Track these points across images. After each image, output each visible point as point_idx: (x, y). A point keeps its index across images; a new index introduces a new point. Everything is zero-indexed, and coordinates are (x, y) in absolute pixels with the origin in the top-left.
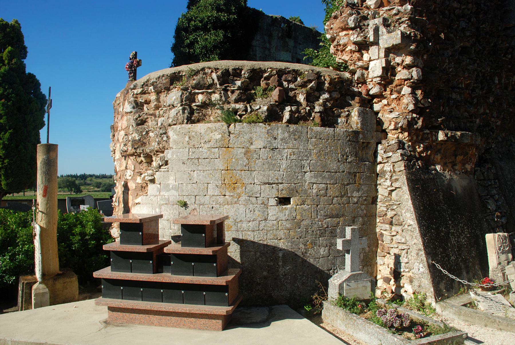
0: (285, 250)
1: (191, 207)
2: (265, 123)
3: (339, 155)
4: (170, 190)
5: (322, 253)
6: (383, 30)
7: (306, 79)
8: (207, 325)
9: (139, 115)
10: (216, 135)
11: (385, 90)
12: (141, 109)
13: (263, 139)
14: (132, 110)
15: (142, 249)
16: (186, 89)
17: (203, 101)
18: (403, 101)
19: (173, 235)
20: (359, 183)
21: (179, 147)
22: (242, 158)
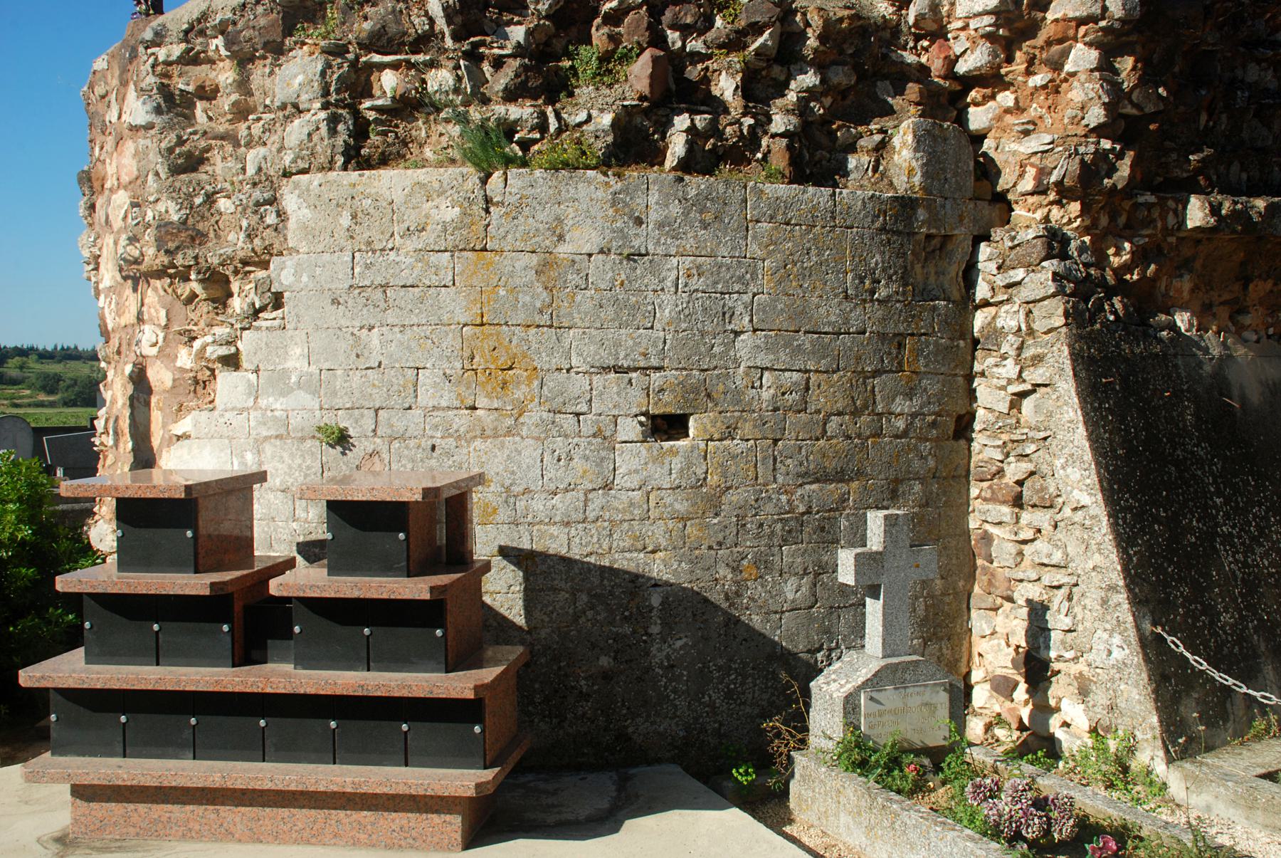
0: (671, 585)
1: (362, 446)
2: (605, 169)
3: (850, 276)
4: (292, 390)
5: (790, 596)
7: (743, 23)
8: (414, 833)
9: (179, 137)
10: (443, 207)
11: (1010, 60)
12: (186, 117)
13: (600, 222)
14: (152, 118)
15: (194, 584)
16: (338, 51)
17: (399, 93)
18: (1069, 96)
19: (301, 539)
20: (913, 368)
22: (529, 285)
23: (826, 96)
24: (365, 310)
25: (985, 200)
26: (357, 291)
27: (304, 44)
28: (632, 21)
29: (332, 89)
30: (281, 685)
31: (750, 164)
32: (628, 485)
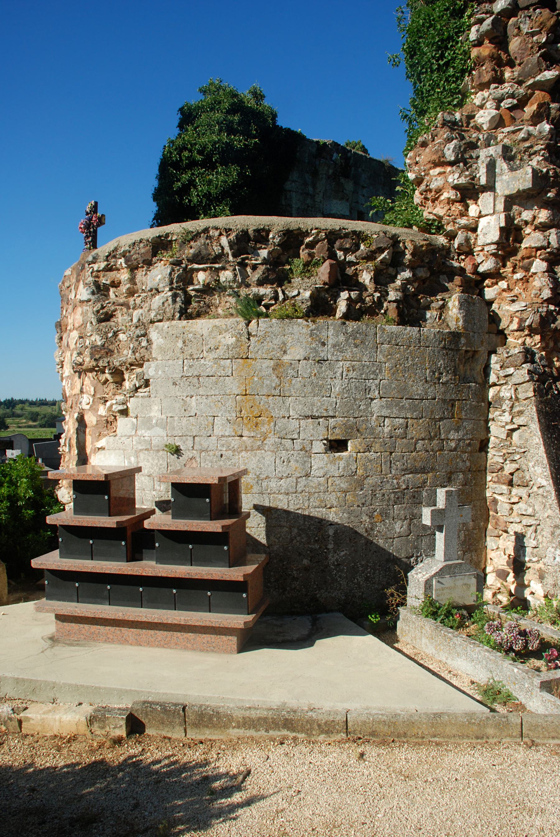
0: (339, 524)
1: (187, 454)
3: (428, 371)
4: (153, 427)
5: (398, 530)
6: (502, 165)
7: (374, 247)
8: (214, 645)
9: (102, 305)
10: (227, 337)
11: (504, 266)
12: (105, 296)
14: (90, 297)
16: (178, 263)
19: (157, 500)
20: (459, 417)
21: (168, 357)
22: (269, 376)
23: (415, 282)
24: (189, 388)
25: (493, 333)
26: (185, 378)
27: (161, 260)
28: (320, 246)
29: (174, 281)
30: (150, 572)
31: (378, 315)
32: (318, 475)
